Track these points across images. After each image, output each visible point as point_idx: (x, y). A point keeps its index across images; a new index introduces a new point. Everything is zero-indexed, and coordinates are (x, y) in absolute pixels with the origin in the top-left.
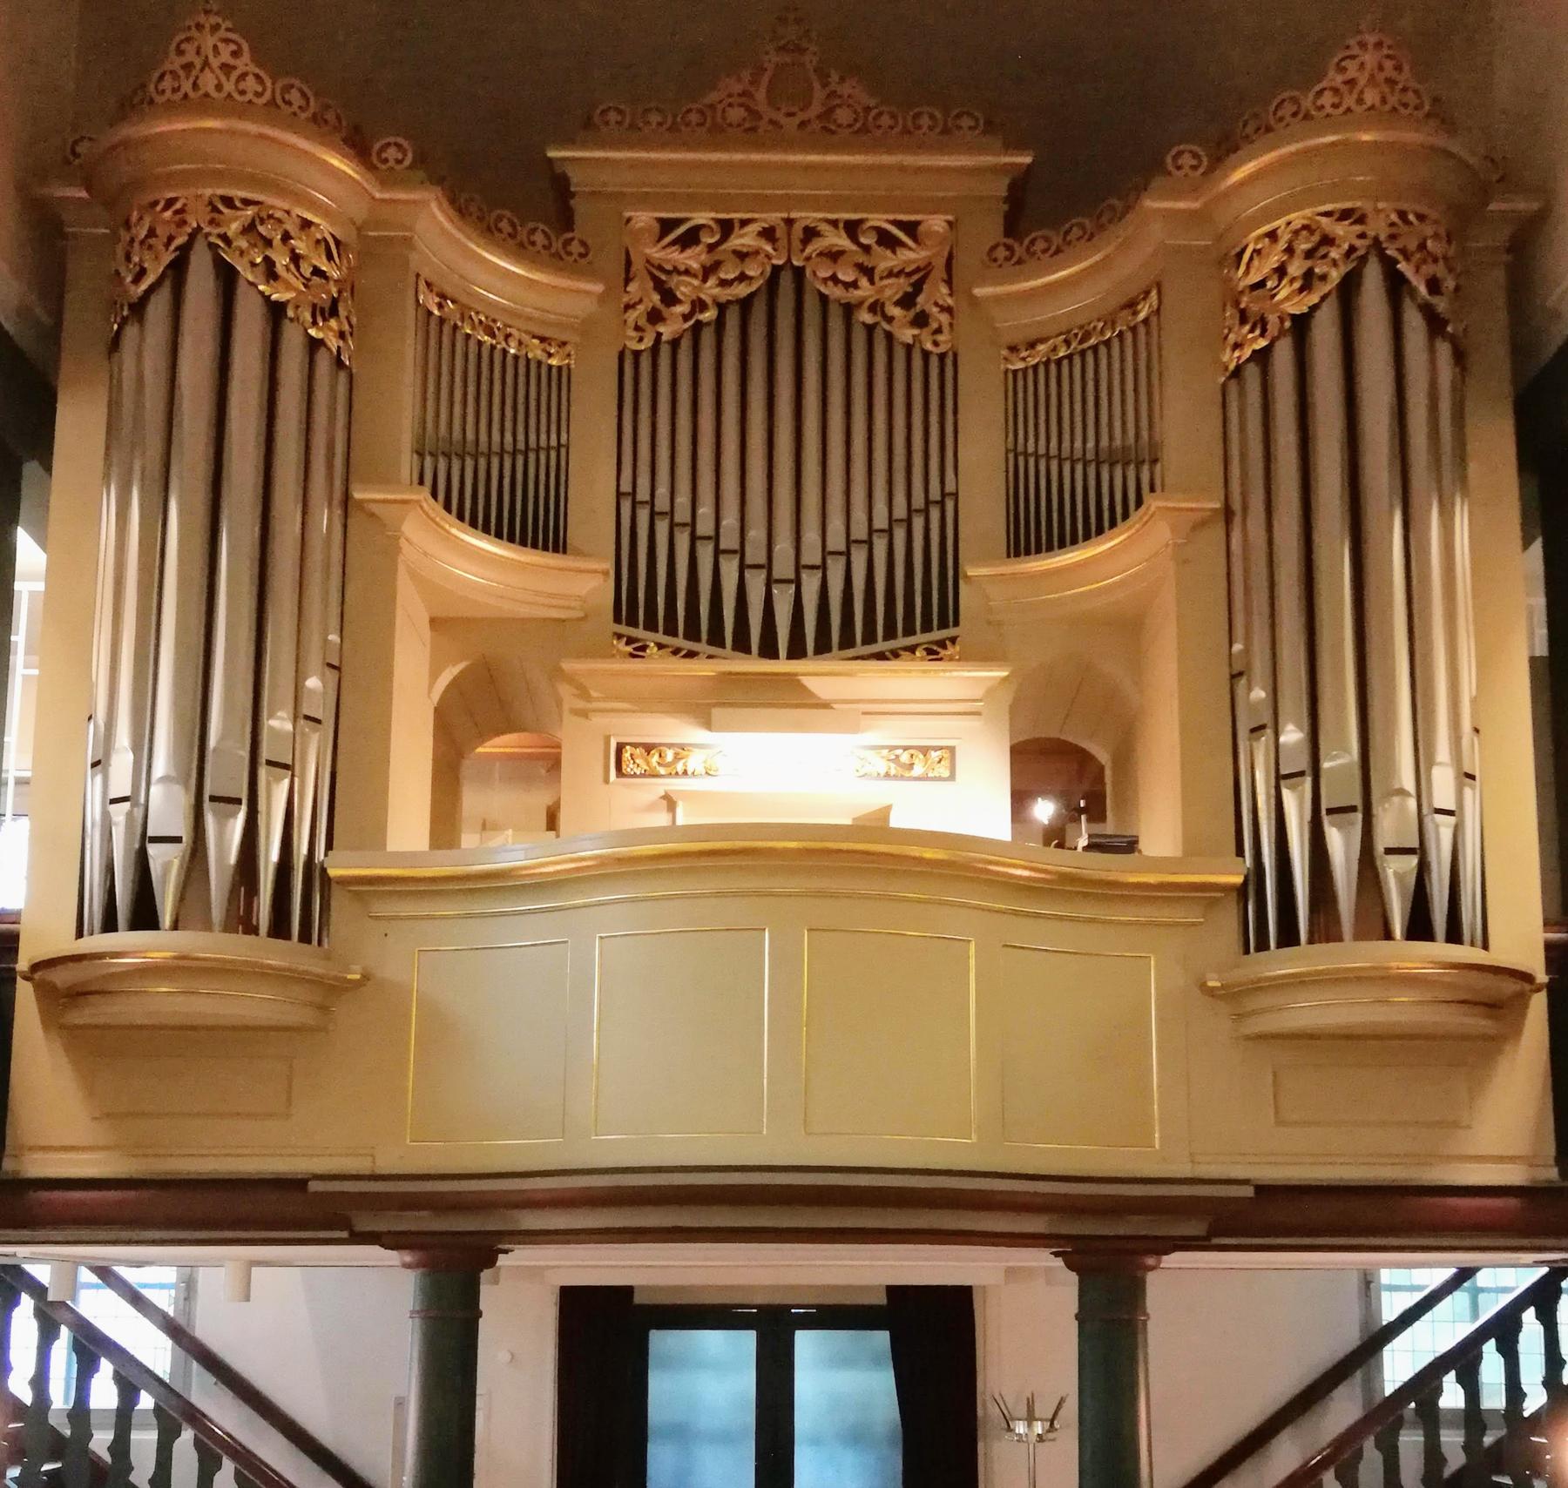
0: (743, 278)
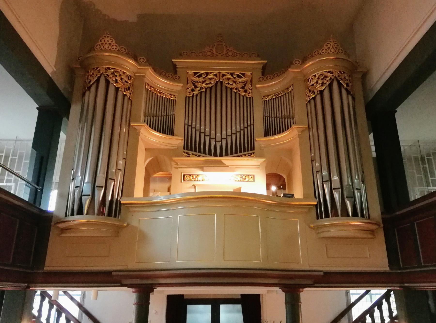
0: (210, 83)
